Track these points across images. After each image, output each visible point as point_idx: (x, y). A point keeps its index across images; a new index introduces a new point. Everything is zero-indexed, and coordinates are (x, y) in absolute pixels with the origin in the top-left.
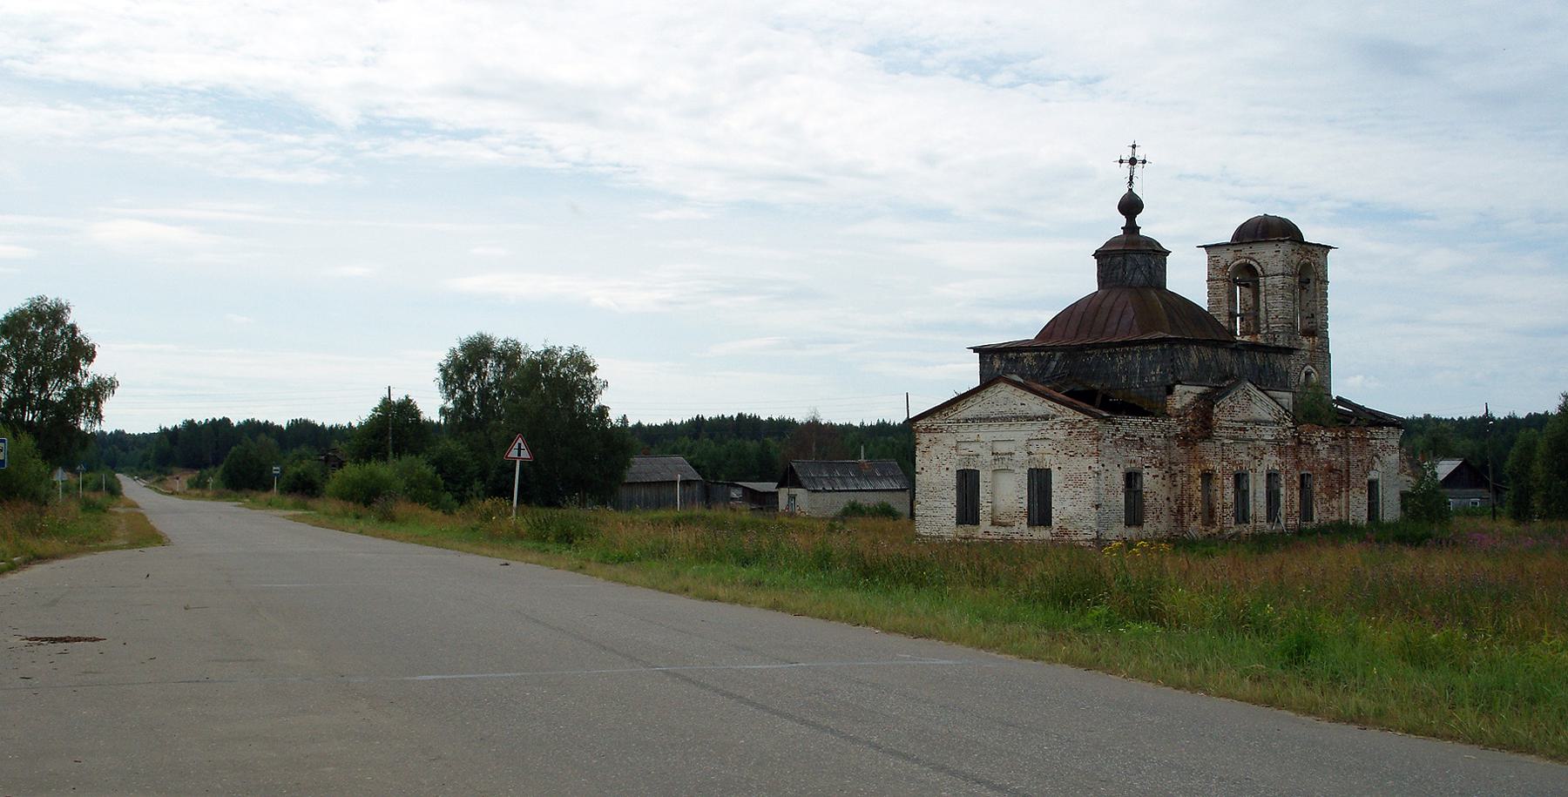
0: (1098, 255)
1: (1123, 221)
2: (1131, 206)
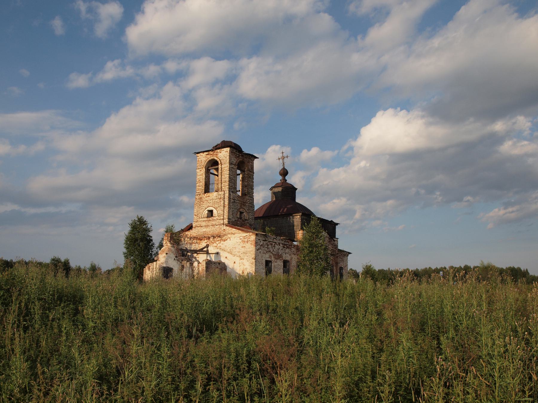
0: (296, 189)
1: (281, 178)
2: (284, 173)
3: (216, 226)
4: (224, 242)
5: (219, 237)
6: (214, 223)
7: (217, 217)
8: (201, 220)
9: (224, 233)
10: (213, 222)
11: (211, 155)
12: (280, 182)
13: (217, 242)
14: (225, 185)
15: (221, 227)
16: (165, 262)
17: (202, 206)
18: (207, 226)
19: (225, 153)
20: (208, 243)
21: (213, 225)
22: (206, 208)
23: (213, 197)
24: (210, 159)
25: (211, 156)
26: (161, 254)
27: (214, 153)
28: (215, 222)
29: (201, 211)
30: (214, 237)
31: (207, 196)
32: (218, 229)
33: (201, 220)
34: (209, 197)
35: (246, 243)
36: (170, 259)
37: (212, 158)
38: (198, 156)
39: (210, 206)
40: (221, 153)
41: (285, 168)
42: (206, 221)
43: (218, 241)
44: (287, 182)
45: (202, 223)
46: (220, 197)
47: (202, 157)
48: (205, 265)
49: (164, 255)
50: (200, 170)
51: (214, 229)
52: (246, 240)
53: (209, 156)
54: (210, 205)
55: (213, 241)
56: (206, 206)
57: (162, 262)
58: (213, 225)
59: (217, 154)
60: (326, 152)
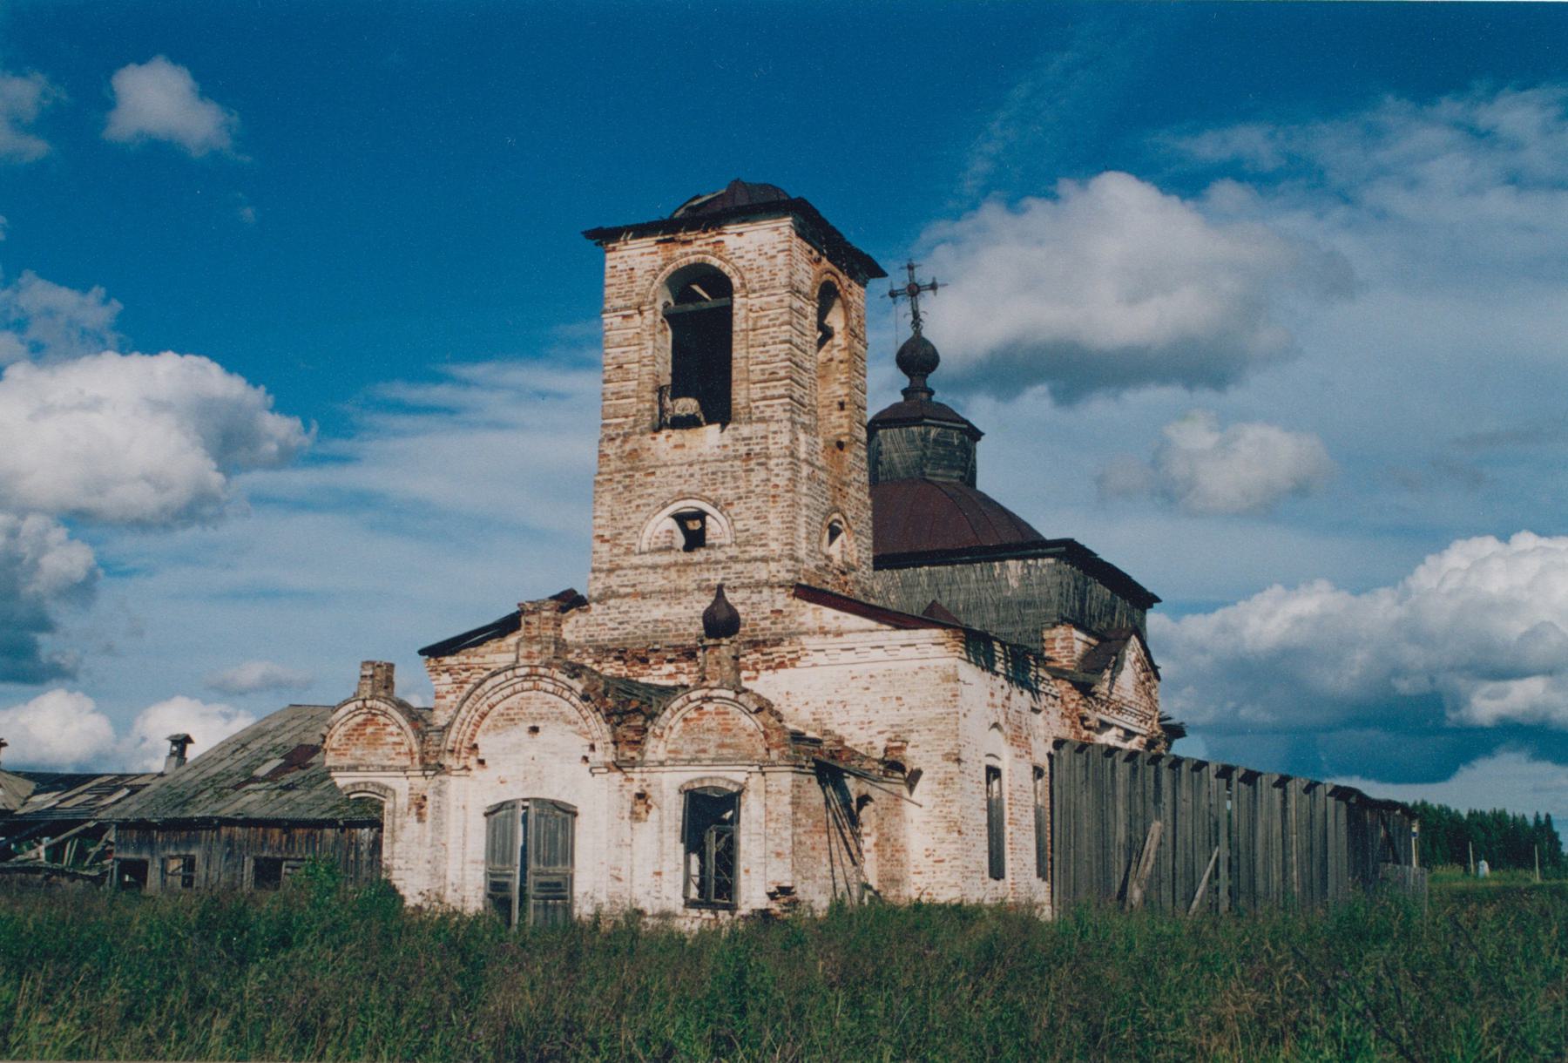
7: (734, 551)
8: (636, 560)
14: (769, 393)
33: (636, 560)
37: (692, 259)
41: (926, 334)
42: (667, 567)
46: (743, 450)
50: (624, 317)
54: (686, 488)
56: (664, 493)
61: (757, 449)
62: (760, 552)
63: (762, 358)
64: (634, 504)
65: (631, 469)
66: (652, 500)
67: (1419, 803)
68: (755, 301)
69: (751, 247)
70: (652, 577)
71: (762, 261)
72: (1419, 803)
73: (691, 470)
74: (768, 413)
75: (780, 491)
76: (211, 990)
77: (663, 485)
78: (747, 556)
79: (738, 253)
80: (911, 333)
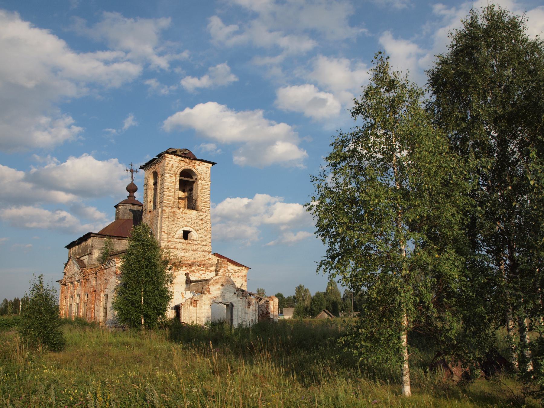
3: (199, 253)
4: (210, 273)
5: (204, 265)
6: (195, 248)
7: (199, 242)
8: (175, 240)
9: (210, 262)
10: (194, 247)
11: (187, 163)
12: (127, 198)
13: (201, 272)
14: (205, 206)
15: (205, 254)
16: (221, 295)
17: (176, 222)
18: (186, 250)
19: (205, 168)
20: (188, 271)
21: (194, 251)
22: (183, 227)
23: (192, 216)
24: (186, 167)
25: (187, 164)
26: (213, 285)
27: (191, 163)
28: (197, 247)
29: (175, 229)
30: (200, 266)
31: (184, 212)
32: (202, 256)
33: (175, 240)
34: (185, 215)
35: (237, 277)
36: (228, 293)
37: (189, 167)
38: (168, 157)
39: (188, 226)
40: (199, 165)
41: (134, 182)
42: (183, 243)
43: (203, 270)
44: (136, 199)
45: (177, 245)
46: (201, 218)
47: (173, 160)
48: (278, 303)
49: (219, 286)
50: (170, 176)
51: (196, 255)
52: (237, 274)
53: (183, 164)
54: (188, 225)
55: (196, 270)
56: (182, 224)
57: (215, 296)
58: (194, 251)
59: (194, 165)
60: (69, 163)
61: (204, 219)
62: (205, 244)
63: (204, 197)
64: (174, 225)
65: (173, 216)
66: (179, 225)
67: (482, 22)
68: (203, 183)
69: (201, 169)
70: (179, 245)
71: (204, 174)
72: (482, 22)
73: (189, 220)
74: (205, 211)
75: (208, 230)
76: (91, 334)
77: (181, 222)
78: (202, 244)
79: (199, 170)
80: (131, 182)
